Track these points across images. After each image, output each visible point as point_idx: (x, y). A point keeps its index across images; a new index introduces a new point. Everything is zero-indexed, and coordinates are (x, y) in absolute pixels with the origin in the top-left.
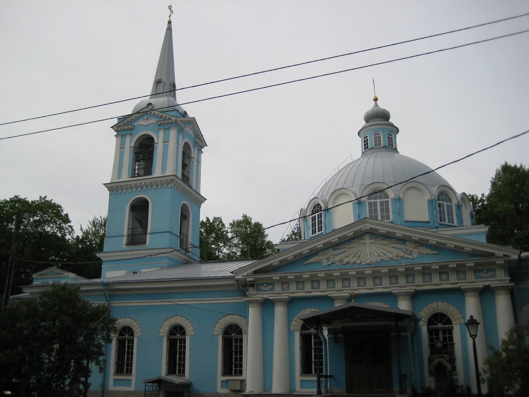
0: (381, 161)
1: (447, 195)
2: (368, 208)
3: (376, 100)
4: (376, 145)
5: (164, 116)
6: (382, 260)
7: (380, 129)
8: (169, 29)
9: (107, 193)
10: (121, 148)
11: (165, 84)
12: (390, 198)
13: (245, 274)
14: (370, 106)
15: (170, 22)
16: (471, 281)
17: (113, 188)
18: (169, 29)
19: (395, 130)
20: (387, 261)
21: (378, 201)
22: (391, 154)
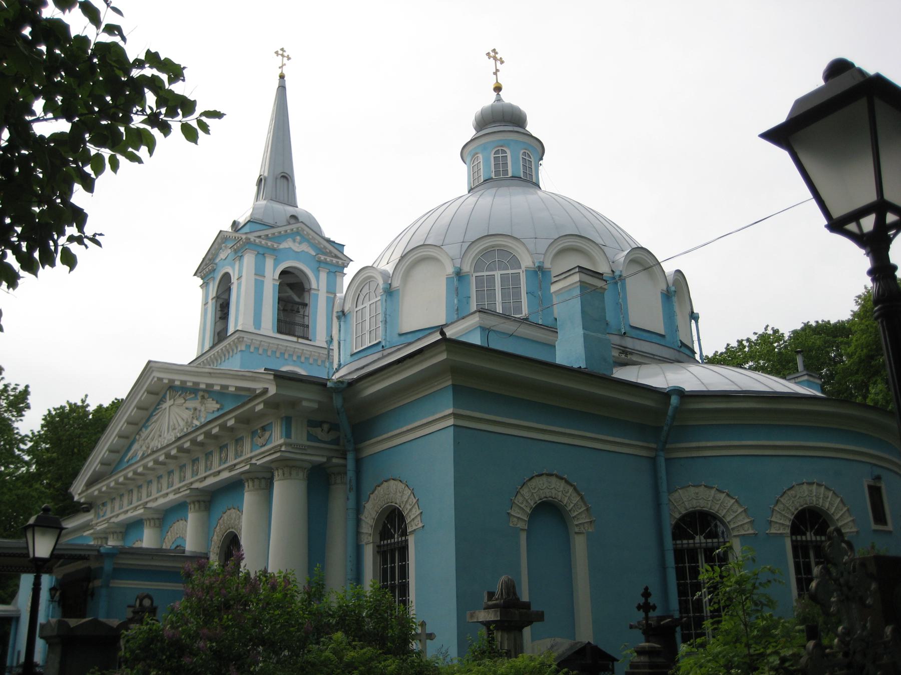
0: (508, 204)
1: (503, 251)
3: (498, 89)
4: (497, 173)
7: (504, 141)
8: (282, 88)
10: (206, 296)
11: (278, 179)
12: (523, 267)
13: (79, 491)
14: (488, 99)
15: (282, 77)
18: (282, 88)
19: (540, 150)
21: (498, 274)
22: (532, 190)
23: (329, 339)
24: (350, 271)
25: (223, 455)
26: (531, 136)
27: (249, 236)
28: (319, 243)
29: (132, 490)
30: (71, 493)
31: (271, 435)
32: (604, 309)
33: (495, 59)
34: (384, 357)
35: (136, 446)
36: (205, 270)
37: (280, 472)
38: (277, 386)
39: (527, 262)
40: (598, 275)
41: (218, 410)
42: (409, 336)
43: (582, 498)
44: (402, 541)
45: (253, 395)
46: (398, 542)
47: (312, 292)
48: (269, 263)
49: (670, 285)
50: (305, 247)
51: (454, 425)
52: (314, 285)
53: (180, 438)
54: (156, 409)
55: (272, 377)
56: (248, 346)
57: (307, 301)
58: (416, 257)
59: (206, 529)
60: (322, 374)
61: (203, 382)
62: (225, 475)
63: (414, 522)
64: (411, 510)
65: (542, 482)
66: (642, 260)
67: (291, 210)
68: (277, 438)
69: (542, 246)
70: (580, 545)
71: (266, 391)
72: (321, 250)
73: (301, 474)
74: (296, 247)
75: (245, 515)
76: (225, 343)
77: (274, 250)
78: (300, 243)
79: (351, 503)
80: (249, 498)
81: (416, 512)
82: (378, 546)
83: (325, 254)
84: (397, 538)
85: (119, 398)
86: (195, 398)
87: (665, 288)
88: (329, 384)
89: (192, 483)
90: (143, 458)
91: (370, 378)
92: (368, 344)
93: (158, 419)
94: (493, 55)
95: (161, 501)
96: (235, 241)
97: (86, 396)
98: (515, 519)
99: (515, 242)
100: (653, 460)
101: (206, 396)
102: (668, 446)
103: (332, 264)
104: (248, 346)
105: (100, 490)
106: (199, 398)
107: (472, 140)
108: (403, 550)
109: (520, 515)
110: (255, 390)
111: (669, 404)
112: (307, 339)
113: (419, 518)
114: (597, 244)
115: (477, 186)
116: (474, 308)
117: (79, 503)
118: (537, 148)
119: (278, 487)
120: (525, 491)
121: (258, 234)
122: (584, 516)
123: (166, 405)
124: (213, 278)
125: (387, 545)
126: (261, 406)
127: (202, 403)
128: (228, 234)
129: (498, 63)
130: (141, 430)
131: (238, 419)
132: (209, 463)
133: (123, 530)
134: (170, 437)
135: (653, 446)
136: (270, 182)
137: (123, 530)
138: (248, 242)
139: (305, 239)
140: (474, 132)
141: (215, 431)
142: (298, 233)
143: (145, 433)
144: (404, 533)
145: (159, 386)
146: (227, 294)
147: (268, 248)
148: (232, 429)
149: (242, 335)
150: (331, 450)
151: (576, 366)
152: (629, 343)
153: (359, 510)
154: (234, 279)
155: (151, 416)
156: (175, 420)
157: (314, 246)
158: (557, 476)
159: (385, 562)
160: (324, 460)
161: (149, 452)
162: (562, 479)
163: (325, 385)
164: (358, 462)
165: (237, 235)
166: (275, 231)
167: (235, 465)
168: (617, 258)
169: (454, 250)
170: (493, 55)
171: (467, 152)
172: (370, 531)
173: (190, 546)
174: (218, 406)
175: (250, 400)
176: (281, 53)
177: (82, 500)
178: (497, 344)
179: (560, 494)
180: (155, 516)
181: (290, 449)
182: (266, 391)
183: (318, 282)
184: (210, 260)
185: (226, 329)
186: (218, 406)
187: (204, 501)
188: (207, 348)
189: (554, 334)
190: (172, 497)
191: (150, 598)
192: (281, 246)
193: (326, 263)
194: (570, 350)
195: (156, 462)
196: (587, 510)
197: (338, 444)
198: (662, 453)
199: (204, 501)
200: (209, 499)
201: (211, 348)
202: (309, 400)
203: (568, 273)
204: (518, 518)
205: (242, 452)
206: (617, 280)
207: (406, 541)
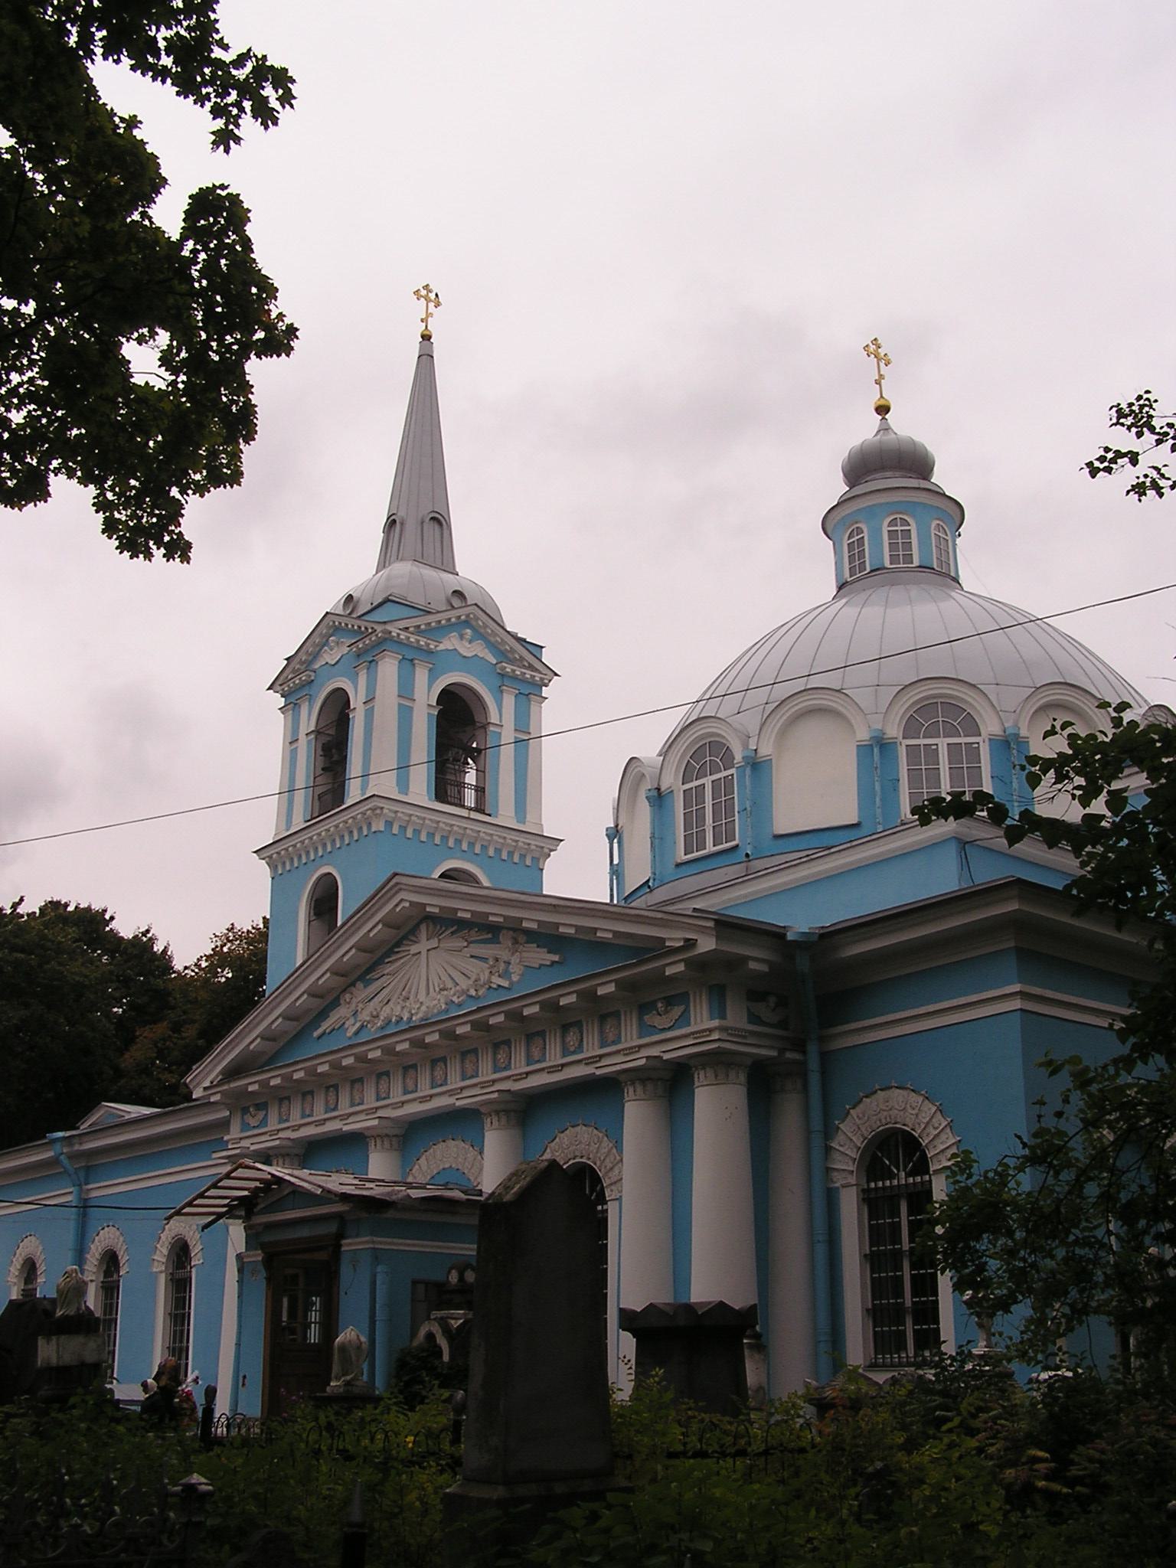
0: (905, 618)
1: (953, 708)
3: (883, 410)
4: (894, 559)
5: (363, 624)
6: (450, 1003)
8: (426, 357)
9: (263, 869)
11: (419, 521)
13: (207, 1084)
14: (863, 430)
15: (426, 337)
16: (631, 1047)
17: (273, 854)
18: (426, 357)
19: (958, 520)
20: (460, 1005)
21: (942, 743)
27: (389, 627)
36: (294, 681)
39: (990, 726)
45: (656, 949)
46: (907, 1185)
47: (492, 728)
50: (478, 649)
52: (494, 718)
55: (711, 924)
56: (389, 824)
67: (450, 582)
71: (690, 944)
72: (504, 655)
74: (467, 649)
77: (431, 652)
78: (470, 642)
82: (863, 1190)
83: (512, 662)
85: (245, 925)
88: (790, 937)
92: (710, 848)
93: (400, 968)
96: (356, 630)
97: (22, 899)
99: (971, 692)
103: (524, 681)
104: (389, 824)
105: (264, 1084)
112: (482, 812)
115: (859, 579)
121: (403, 624)
124: (311, 699)
125: (884, 1188)
130: (353, 984)
131: (628, 987)
136: (411, 528)
139: (480, 635)
142: (467, 623)
143: (361, 992)
147: (419, 649)
154: (357, 701)
157: (493, 647)
160: (775, 1054)
163: (782, 936)
164: (825, 1057)
166: (432, 619)
176: (428, 295)
180: (396, 1131)
181: (725, 1036)
183: (501, 712)
184: (301, 663)
188: (298, 823)
192: (441, 647)
193: (515, 678)
197: (786, 1029)
200: (527, 1110)
202: (758, 958)
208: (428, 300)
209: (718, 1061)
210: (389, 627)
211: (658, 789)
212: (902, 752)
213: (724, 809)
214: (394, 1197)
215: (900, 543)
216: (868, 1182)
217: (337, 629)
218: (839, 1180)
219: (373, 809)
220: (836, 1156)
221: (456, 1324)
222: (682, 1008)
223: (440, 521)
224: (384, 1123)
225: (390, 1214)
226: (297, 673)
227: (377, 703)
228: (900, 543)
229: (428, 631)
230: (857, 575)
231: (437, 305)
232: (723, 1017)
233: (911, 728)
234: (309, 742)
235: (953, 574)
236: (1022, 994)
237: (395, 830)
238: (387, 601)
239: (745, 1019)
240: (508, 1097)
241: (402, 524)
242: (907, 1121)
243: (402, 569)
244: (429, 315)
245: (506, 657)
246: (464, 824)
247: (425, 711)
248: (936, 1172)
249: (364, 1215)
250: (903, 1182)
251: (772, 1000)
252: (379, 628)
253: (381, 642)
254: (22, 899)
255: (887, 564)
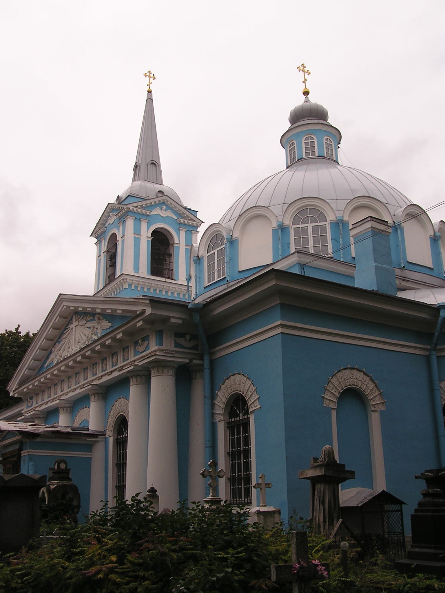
0: (314, 179)
2: (293, 238)
3: (306, 93)
7: (310, 130)
8: (150, 100)
11: (148, 164)
13: (14, 389)
14: (299, 101)
15: (150, 92)
18: (150, 100)
19: (338, 138)
21: (310, 226)
23: (188, 277)
24: (202, 230)
25: (114, 360)
26: (331, 126)
27: (129, 206)
28: (179, 210)
29: (50, 387)
30: (7, 391)
31: (149, 343)
32: (389, 247)
33: (304, 71)
34: (228, 288)
35: (52, 356)
37: (156, 370)
38: (152, 307)
39: (331, 217)
40: (385, 223)
41: (110, 327)
42: (246, 272)
43: (376, 386)
44: (245, 419)
46: (242, 419)
47: (175, 245)
48: (144, 225)
49: (437, 231)
51: (280, 303)
52: (176, 240)
53: (83, 349)
54: (65, 329)
55: (148, 302)
56: (130, 285)
57: (171, 253)
58: (251, 214)
59: (104, 415)
60: (186, 299)
61: (99, 308)
62: (116, 374)
63: (254, 405)
64: (251, 396)
65: (347, 373)
66: (416, 214)
67: (159, 187)
68: (153, 347)
69: (342, 205)
70: (375, 419)
71: (144, 312)
73: (171, 372)
74: (163, 214)
75: (131, 403)
76: (114, 283)
77: (148, 216)
78: (165, 211)
79: (208, 393)
80: (134, 390)
81: (256, 396)
83: (184, 218)
84: (241, 417)
86: (93, 320)
87: (432, 234)
88: (190, 306)
89: (92, 381)
90: (58, 364)
91: (220, 301)
92: (217, 279)
93: (67, 336)
94: (302, 69)
95: (71, 394)
96: (120, 210)
97: (19, 326)
98: (328, 401)
100: (428, 358)
101: (101, 317)
102: (438, 347)
103: (189, 225)
104: (130, 285)
106: (96, 319)
107: (288, 131)
108: (246, 425)
109: (331, 398)
110: (136, 311)
111: (439, 316)
113: (257, 401)
114: (382, 203)
115: (293, 164)
116: (293, 250)
117: (13, 398)
118: (336, 135)
119: (155, 381)
120: (334, 380)
122: (378, 398)
123: (72, 326)
124: (105, 238)
125: (234, 421)
126: (141, 323)
127: (99, 323)
128: (114, 206)
129: (306, 74)
130: (55, 344)
132: (104, 366)
133: (45, 416)
134: (75, 348)
135: (429, 347)
136: (143, 168)
137: (45, 416)
138: (129, 211)
139: (169, 208)
140: (290, 125)
141: (108, 342)
143: (58, 346)
144: (247, 413)
145: (68, 312)
146: (115, 248)
147: (143, 214)
148: (120, 341)
149: (126, 277)
150: (192, 353)
151: (370, 289)
152: (408, 274)
153: (213, 396)
154: (119, 238)
155: (62, 334)
156: (79, 337)
157: (176, 212)
158: (358, 370)
159: (233, 434)
160: (187, 361)
161: (62, 359)
162: (361, 371)
164: (212, 363)
165: (120, 206)
166: (146, 202)
167: (123, 366)
168: (397, 212)
169: (277, 210)
170: (302, 69)
171: (285, 140)
172: (222, 406)
173: (93, 426)
174: (110, 324)
175: (134, 319)
176: (150, 75)
177: (16, 396)
178: (309, 273)
179: (360, 382)
180: (67, 405)
182: (144, 312)
183: (179, 239)
184: (102, 224)
185: (114, 273)
186: (110, 324)
187: (101, 393)
188: (101, 287)
189: (353, 268)
190: (78, 391)
191: (66, 463)
192: (152, 213)
193: (185, 224)
194: (365, 279)
195: (67, 366)
196: (380, 394)
198: (434, 352)
199: (101, 393)
200: (107, 392)
201: (104, 287)
202: (176, 318)
203: (363, 221)
204: (330, 400)
205: (128, 357)
206: (397, 227)
207: (248, 418)
208: (150, 77)
209: (159, 365)
210: (129, 206)
211: (198, 256)
212: (292, 231)
213: (221, 262)
214: (37, 432)
215: (310, 147)
216: (229, 419)
217: (113, 210)
218: (218, 418)
219: (123, 280)
220: (216, 407)
221: (52, 487)
222: (147, 342)
223: (155, 164)
224: (62, 402)
225: (38, 439)
226: (100, 228)
227: (125, 237)
228: (310, 147)
229: (147, 207)
230: (293, 162)
231: (154, 79)
232: (161, 344)
233: (296, 220)
234: (104, 256)
235: (334, 159)
236: (282, 326)
237: (133, 288)
238: (129, 196)
239: (173, 344)
240: (96, 387)
241: (140, 166)
242: (242, 390)
243: (137, 183)
244: (150, 83)
245: (181, 216)
246: (163, 284)
247: (146, 239)
248: (252, 412)
249: (27, 440)
250: (241, 418)
251: (188, 337)
252: (125, 207)
253: (127, 212)
254: (19, 326)
255: (304, 156)
